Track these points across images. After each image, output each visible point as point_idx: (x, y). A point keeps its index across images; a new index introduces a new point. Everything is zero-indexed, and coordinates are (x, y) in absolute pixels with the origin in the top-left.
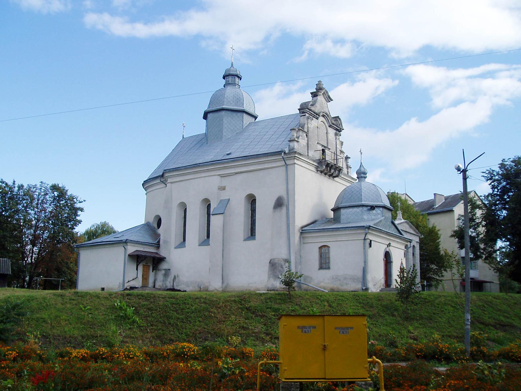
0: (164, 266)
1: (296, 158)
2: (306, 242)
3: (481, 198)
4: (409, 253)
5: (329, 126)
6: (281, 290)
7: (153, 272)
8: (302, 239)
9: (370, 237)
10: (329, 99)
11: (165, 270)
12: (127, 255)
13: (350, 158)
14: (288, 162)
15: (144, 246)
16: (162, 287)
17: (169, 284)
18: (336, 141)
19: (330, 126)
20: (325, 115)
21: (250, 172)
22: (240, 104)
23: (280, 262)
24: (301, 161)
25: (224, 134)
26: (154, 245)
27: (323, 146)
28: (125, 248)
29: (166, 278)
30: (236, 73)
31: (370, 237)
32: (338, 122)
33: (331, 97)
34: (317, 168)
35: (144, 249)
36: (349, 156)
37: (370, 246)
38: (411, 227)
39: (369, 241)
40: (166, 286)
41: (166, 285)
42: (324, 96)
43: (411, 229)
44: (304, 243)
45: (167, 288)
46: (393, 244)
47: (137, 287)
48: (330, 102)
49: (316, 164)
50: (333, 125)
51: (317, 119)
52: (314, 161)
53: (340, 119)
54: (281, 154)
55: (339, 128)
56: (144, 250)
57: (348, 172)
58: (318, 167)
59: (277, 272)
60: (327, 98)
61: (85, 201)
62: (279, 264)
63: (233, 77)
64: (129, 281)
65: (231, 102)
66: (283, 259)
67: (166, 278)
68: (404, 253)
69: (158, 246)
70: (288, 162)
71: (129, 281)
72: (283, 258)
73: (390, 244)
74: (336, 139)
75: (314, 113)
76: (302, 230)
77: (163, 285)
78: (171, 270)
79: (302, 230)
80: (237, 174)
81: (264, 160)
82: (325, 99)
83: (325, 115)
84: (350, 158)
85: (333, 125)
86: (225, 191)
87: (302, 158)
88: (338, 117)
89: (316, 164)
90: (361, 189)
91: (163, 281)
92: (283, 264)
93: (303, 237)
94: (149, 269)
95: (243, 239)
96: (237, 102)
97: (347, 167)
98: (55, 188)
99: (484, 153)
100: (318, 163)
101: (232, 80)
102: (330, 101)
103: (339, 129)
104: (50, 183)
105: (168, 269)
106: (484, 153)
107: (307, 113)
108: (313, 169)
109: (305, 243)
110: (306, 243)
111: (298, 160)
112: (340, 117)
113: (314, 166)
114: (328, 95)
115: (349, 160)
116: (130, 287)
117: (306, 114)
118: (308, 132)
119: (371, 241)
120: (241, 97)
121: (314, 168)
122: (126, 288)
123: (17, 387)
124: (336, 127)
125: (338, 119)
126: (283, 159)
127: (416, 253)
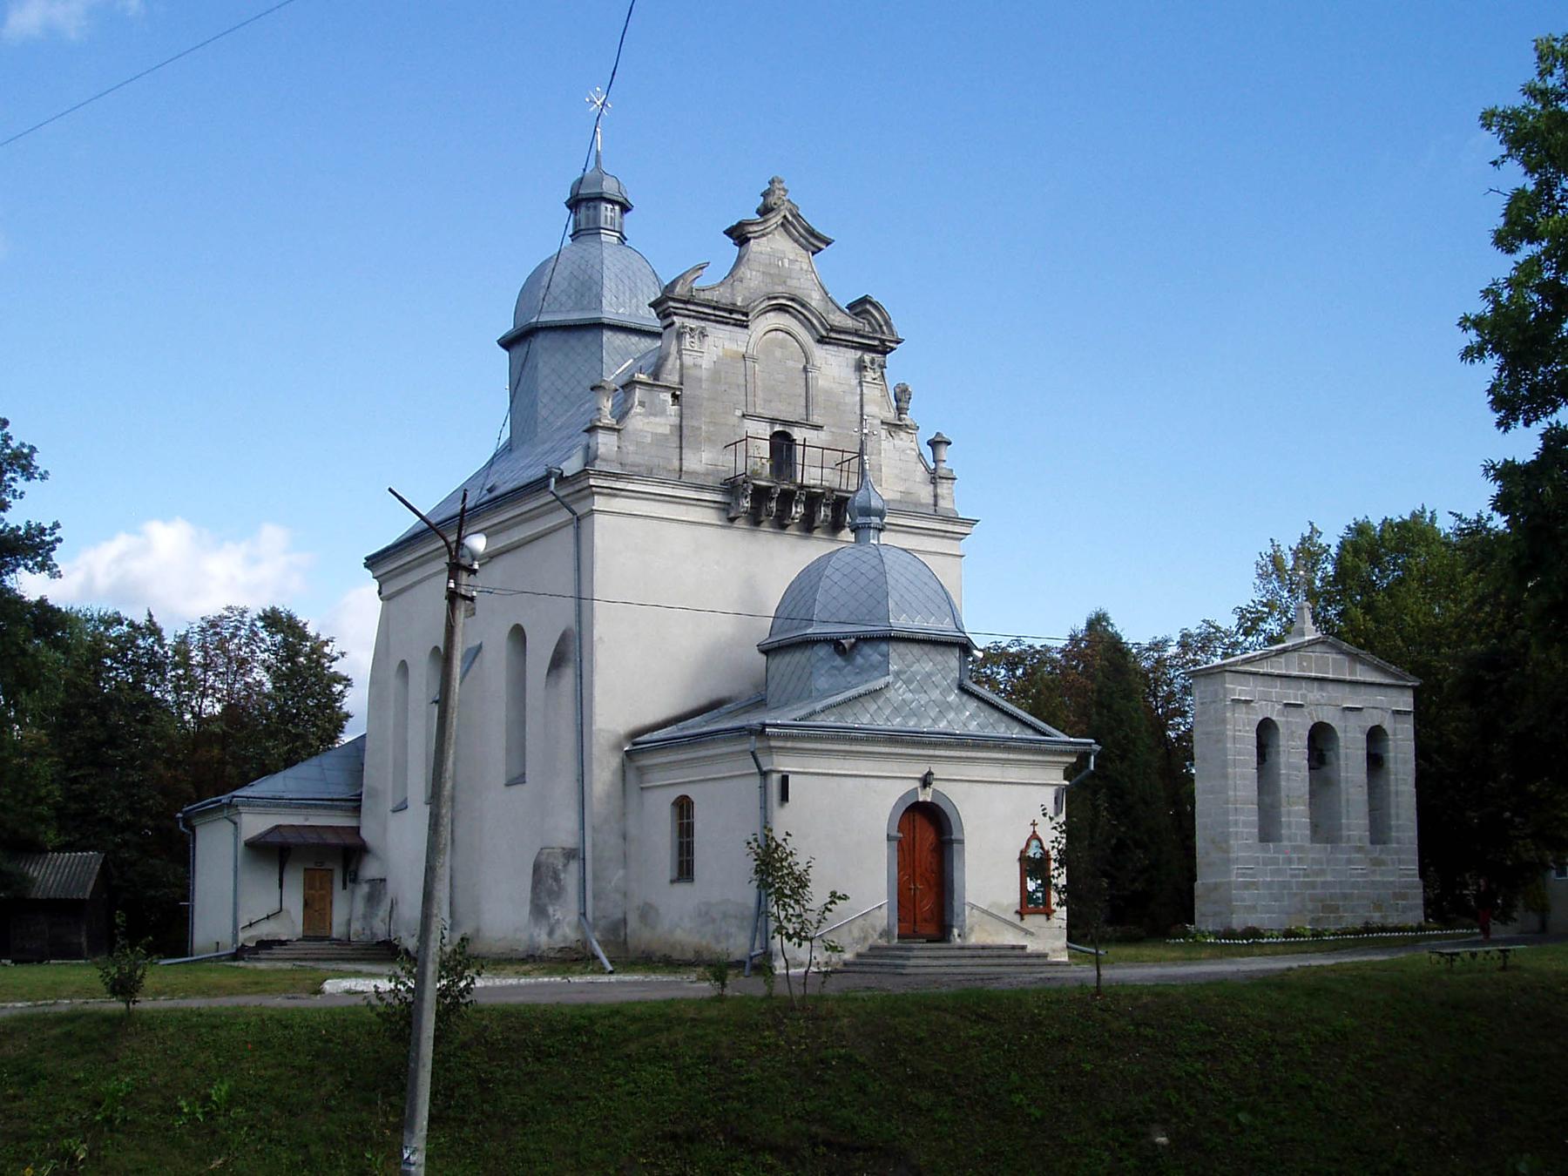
0: (370, 870)
1: (594, 489)
2: (648, 785)
3: (786, 627)
4: (1342, 762)
8: (631, 776)
9: (784, 764)
10: (812, 240)
11: (372, 881)
13: (949, 443)
14: (580, 509)
17: (381, 924)
19: (822, 340)
20: (789, 303)
23: (551, 860)
25: (544, 412)
27: (773, 421)
28: (235, 824)
30: (599, 191)
31: (784, 764)
32: (873, 316)
33: (818, 229)
34: (724, 508)
35: (307, 820)
36: (947, 436)
37: (784, 797)
38: (1354, 658)
39: (776, 778)
40: (373, 935)
41: (371, 929)
42: (787, 231)
43: (1359, 667)
45: (375, 940)
46: (939, 770)
47: (284, 938)
48: (820, 249)
50: (833, 335)
51: (747, 327)
52: (713, 489)
53: (874, 305)
54: (548, 486)
55: (874, 338)
56: (307, 823)
57: (936, 496)
58: (729, 504)
59: (543, 895)
61: (343, 654)
63: (591, 204)
64: (251, 925)
65: (564, 298)
66: (564, 849)
68: (1056, 798)
69: (355, 805)
70: (580, 509)
71: (251, 925)
73: (930, 773)
74: (860, 383)
75: (714, 308)
76: (635, 744)
77: (364, 929)
78: (388, 882)
79: (635, 744)
82: (796, 241)
83: (789, 303)
85: (833, 335)
86: (474, 618)
87: (631, 487)
88: (865, 300)
90: (884, 574)
93: (638, 768)
94: (331, 882)
96: (582, 296)
98: (273, 620)
100: (726, 492)
102: (823, 246)
107: (676, 314)
108: (711, 516)
111: (615, 496)
112: (875, 299)
113: (712, 505)
114: (803, 227)
115: (944, 452)
116: (257, 943)
117: (675, 318)
119: (785, 780)
120: (596, 277)
121: (712, 511)
122: (243, 945)
123: (1194, 1076)
124: (856, 339)
125: (868, 307)
127: (1391, 754)
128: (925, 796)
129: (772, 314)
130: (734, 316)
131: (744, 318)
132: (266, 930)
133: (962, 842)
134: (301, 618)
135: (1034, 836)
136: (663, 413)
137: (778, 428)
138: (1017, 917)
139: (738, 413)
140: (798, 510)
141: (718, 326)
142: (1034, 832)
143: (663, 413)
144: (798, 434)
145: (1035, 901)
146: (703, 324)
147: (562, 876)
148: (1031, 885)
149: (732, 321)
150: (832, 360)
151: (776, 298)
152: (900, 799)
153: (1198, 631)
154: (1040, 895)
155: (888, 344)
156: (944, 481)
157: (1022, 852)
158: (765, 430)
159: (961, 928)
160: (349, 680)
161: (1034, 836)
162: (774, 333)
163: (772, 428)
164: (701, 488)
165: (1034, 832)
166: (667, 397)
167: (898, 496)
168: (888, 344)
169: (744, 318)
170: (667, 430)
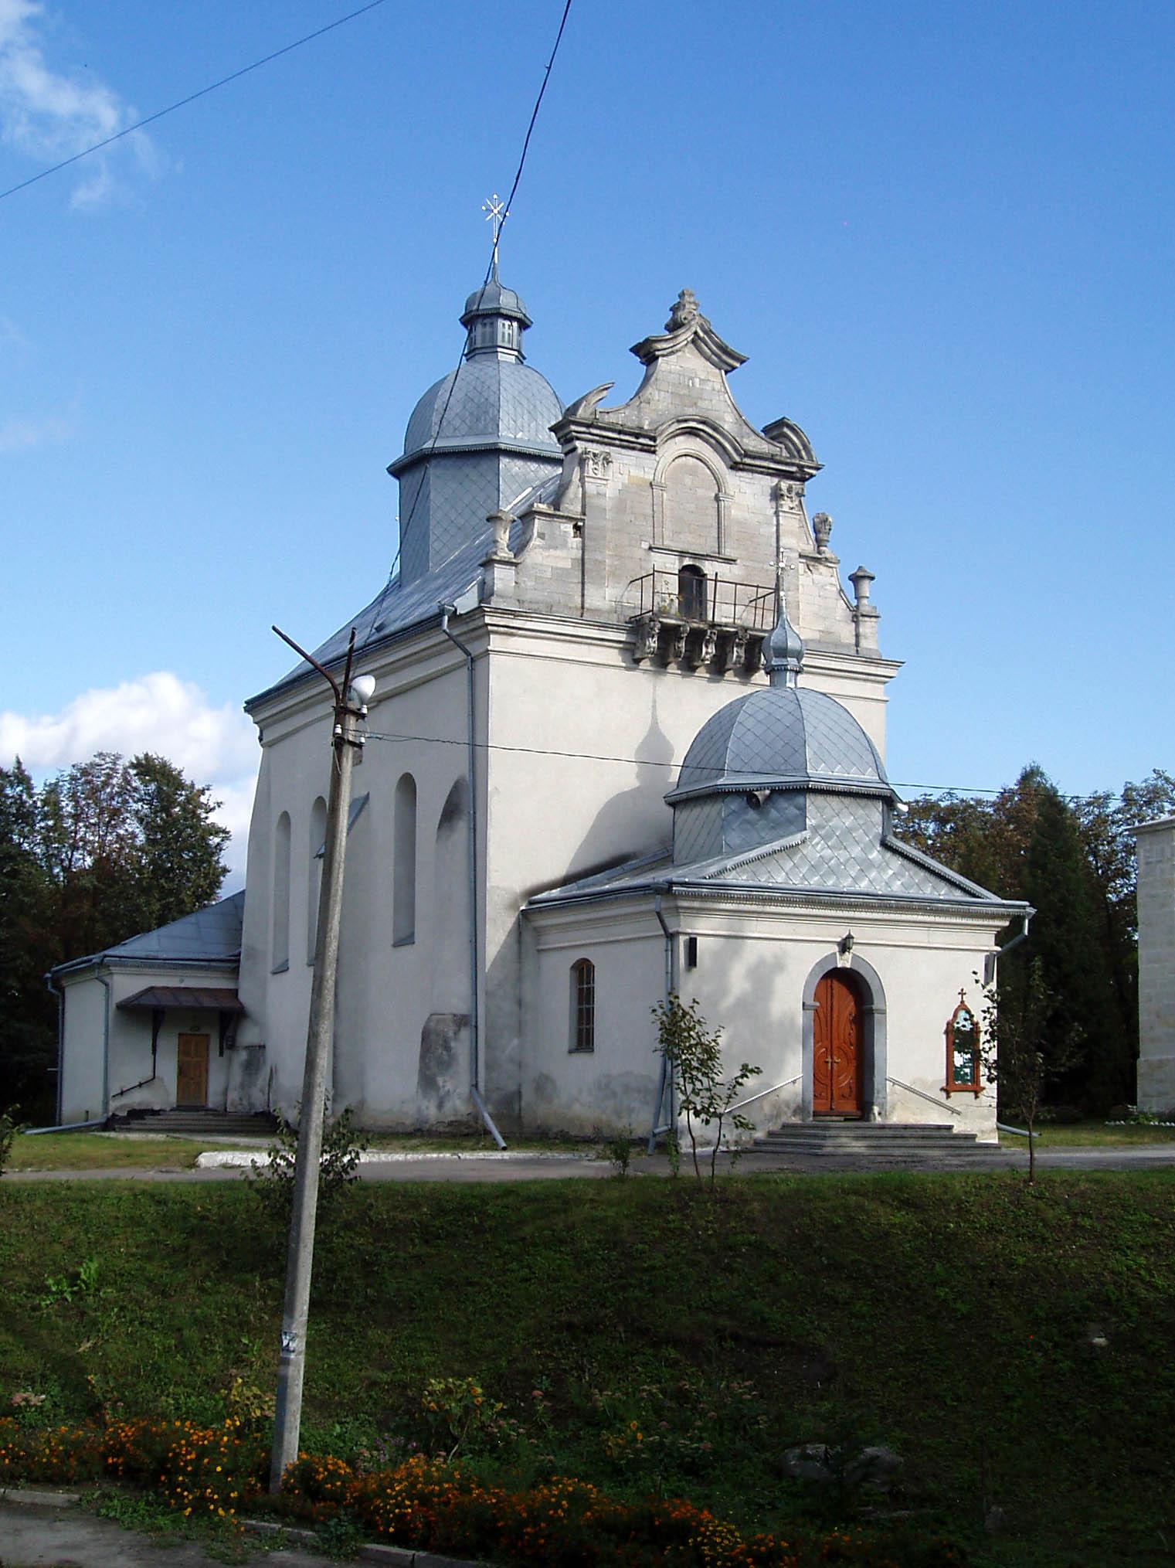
5: (732, 468)
6: (441, 1129)
7: (221, 1054)
10: (724, 357)
11: (250, 1048)
12: (112, 1007)
15: (180, 972)
16: (240, 1107)
18: (778, 521)
20: (700, 426)
21: (424, 683)
22: (485, 427)
24: (521, 636)
26: (219, 964)
27: (682, 554)
28: (107, 985)
29: (250, 1075)
35: (182, 981)
40: (251, 1105)
44: (539, 951)
45: (253, 1111)
46: (859, 933)
47: (157, 1108)
49: (623, 637)
50: (748, 461)
56: (182, 985)
57: (857, 636)
60: (716, 355)
61: (219, 804)
62: (438, 1035)
63: (487, 321)
64: (122, 1093)
66: (455, 1015)
67: (250, 1075)
69: (232, 965)
71: (122, 1093)
72: (455, 1012)
73: (850, 937)
74: (777, 513)
76: (531, 903)
77: (241, 1099)
80: (382, 703)
81: (423, 646)
83: (700, 426)
84: (872, 578)
85: (748, 461)
88: (781, 423)
89: (623, 637)
91: (242, 1086)
92: (451, 1034)
95: (392, 942)
97: (855, 616)
99: (274, 628)
100: (630, 632)
101: (484, 335)
103: (794, 469)
104: (131, 753)
105: (260, 1047)
106: (274, 628)
107: (578, 439)
108: (614, 656)
109: (542, 950)
110: (549, 949)
115: (866, 587)
116: (129, 1112)
118: (584, 514)
121: (616, 651)
122: (114, 1115)
125: (785, 430)
126: (755, 600)
128: (845, 962)
129: (681, 438)
130: (641, 440)
131: (652, 443)
132: (138, 1099)
133: (884, 1012)
134: (176, 765)
135: (963, 1006)
136: (564, 545)
137: (687, 562)
138: (944, 1094)
139: (645, 546)
140: (709, 651)
141: (623, 451)
142: (962, 1002)
143: (564, 545)
144: (709, 568)
145: (962, 1078)
146: (607, 449)
147: (453, 1044)
148: (959, 1059)
149: (639, 446)
150: (745, 487)
151: (686, 421)
152: (817, 964)
153: (1144, 785)
154: (967, 1070)
155: (806, 470)
156: (866, 619)
157: (948, 1024)
158: (674, 564)
159: (882, 1106)
160: (228, 833)
161: (963, 1006)
162: (684, 458)
163: (681, 562)
164: (604, 626)
165: (962, 1002)
166: (569, 528)
167: (816, 636)
168: (806, 470)
169: (652, 443)
170: (568, 564)
